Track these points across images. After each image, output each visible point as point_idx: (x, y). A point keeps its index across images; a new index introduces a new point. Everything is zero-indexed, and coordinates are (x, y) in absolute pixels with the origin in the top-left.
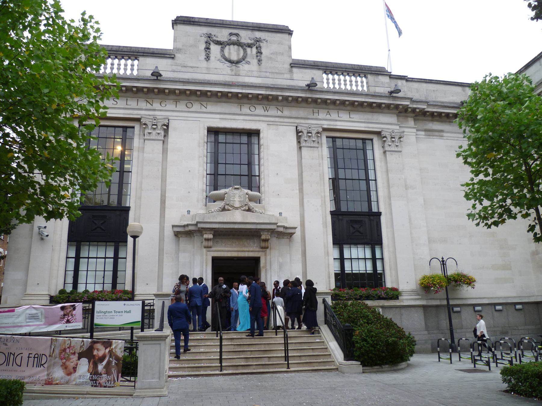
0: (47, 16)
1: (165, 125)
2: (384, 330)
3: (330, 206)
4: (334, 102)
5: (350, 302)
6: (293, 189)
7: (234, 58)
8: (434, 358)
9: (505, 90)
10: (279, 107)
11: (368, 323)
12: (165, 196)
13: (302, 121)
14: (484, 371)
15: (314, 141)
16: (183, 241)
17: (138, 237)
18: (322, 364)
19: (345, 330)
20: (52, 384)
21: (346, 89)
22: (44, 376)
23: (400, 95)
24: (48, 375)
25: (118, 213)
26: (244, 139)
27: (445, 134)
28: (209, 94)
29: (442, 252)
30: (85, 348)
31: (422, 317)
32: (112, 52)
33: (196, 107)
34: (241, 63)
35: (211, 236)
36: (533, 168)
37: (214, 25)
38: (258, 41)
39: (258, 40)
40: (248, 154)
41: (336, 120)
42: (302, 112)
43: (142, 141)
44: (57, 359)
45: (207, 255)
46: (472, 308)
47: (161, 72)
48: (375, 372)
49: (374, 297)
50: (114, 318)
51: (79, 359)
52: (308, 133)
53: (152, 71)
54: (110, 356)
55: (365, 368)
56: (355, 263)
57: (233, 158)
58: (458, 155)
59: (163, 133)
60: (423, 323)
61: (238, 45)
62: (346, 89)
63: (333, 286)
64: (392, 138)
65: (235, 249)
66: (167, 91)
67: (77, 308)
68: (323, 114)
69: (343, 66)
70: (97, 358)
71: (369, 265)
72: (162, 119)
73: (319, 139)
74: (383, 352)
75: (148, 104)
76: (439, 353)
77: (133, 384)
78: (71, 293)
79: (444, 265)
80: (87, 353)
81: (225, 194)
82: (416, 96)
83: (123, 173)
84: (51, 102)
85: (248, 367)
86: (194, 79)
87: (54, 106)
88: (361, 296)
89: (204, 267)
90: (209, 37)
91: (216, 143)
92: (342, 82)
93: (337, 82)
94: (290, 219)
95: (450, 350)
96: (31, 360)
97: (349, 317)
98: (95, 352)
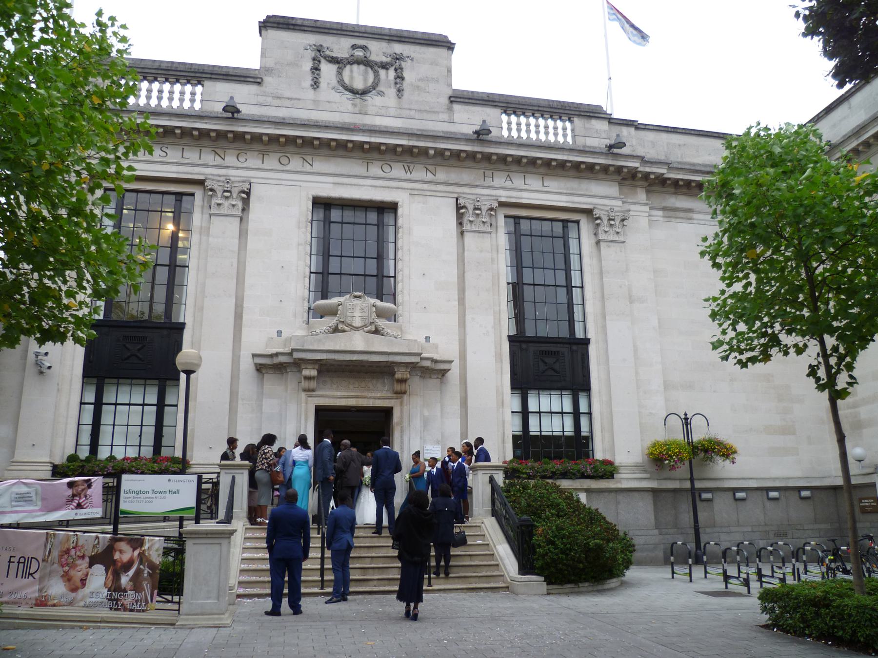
0: (45, 15)
1: (244, 192)
2: (582, 526)
3: (507, 328)
4: (518, 160)
5: (532, 482)
6: (449, 298)
7: (359, 85)
8: (665, 573)
9: (777, 150)
10: (429, 167)
11: (558, 516)
12: (242, 307)
13: (467, 190)
14: (739, 595)
15: (484, 223)
16: (270, 379)
17: (193, 372)
18: (484, 579)
19: (521, 526)
20: (46, 605)
21: (538, 139)
22: (34, 592)
23: (624, 151)
24: (40, 590)
25: (165, 332)
26: (373, 217)
27: (695, 216)
28: (316, 142)
29: (686, 404)
30: (100, 549)
31: (650, 507)
32: (160, 72)
33: (296, 163)
34: (369, 95)
35: (314, 373)
36: (819, 275)
37: (326, 31)
38: (397, 59)
39: (398, 58)
40: (378, 241)
41: (521, 190)
42: (466, 176)
43: (206, 216)
44: (56, 565)
45: (307, 403)
46: (731, 494)
47: (239, 106)
48: (567, 594)
49: (574, 474)
50: (151, 502)
51: (91, 565)
52: (475, 209)
53: (224, 105)
54: (141, 563)
55: (551, 587)
56: (545, 420)
57: (353, 247)
58: (703, 254)
59: (240, 205)
60: (652, 517)
61: (365, 65)
62: (538, 139)
63: (509, 456)
64: (610, 220)
65: (353, 394)
66: (248, 137)
67: (94, 485)
68: (499, 180)
69: (535, 103)
70: (120, 564)
71: (569, 422)
72: (239, 182)
73: (493, 219)
74: (580, 562)
75: (217, 157)
76: (672, 564)
77: (176, 607)
78: (88, 460)
79: (687, 424)
80: (104, 557)
81: (339, 305)
82: (650, 154)
83: (175, 268)
84: (41, 157)
85: (365, 583)
86: (293, 119)
87: (46, 167)
88: (554, 473)
89: (303, 422)
90: (319, 51)
91: (327, 222)
92: (533, 128)
93: (523, 127)
94: (443, 347)
95: (690, 561)
96: (14, 566)
97: (529, 505)
98: (117, 556)
